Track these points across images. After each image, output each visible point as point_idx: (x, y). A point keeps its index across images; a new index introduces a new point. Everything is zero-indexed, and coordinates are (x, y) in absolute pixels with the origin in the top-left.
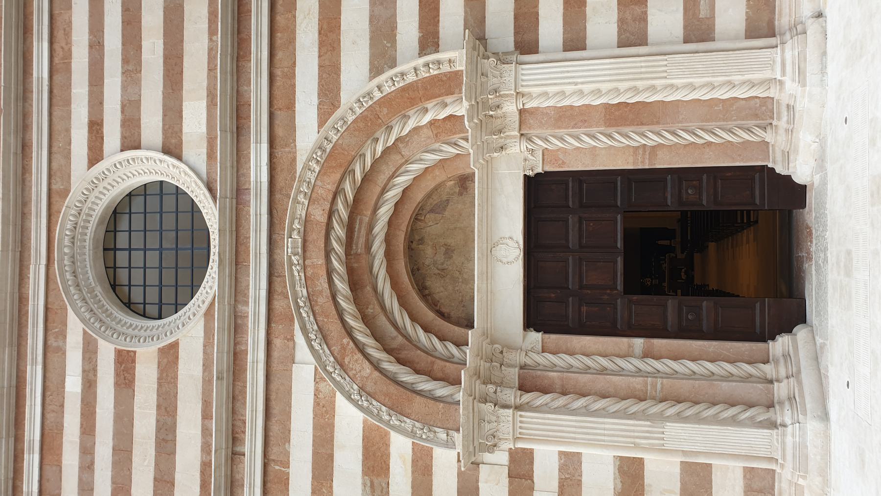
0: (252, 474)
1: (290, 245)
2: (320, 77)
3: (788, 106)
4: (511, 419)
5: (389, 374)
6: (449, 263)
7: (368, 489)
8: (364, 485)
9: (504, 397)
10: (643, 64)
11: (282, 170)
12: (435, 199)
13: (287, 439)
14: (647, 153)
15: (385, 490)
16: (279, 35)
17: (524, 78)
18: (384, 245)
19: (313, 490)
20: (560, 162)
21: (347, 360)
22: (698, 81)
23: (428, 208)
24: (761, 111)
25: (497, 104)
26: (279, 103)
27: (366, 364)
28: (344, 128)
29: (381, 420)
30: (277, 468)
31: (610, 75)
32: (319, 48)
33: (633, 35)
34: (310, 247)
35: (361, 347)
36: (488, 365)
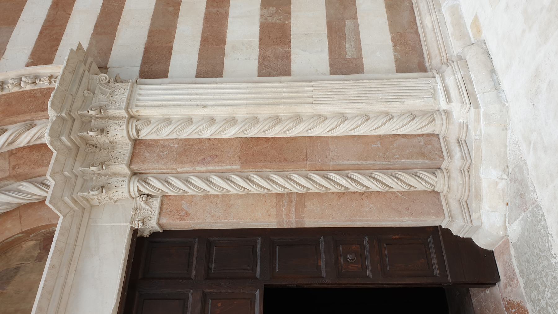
3: (458, 141)
10: (285, 90)
14: (293, 204)
17: (141, 92)
20: (183, 213)
22: (348, 109)
24: (426, 151)
31: (247, 99)
33: (275, 57)
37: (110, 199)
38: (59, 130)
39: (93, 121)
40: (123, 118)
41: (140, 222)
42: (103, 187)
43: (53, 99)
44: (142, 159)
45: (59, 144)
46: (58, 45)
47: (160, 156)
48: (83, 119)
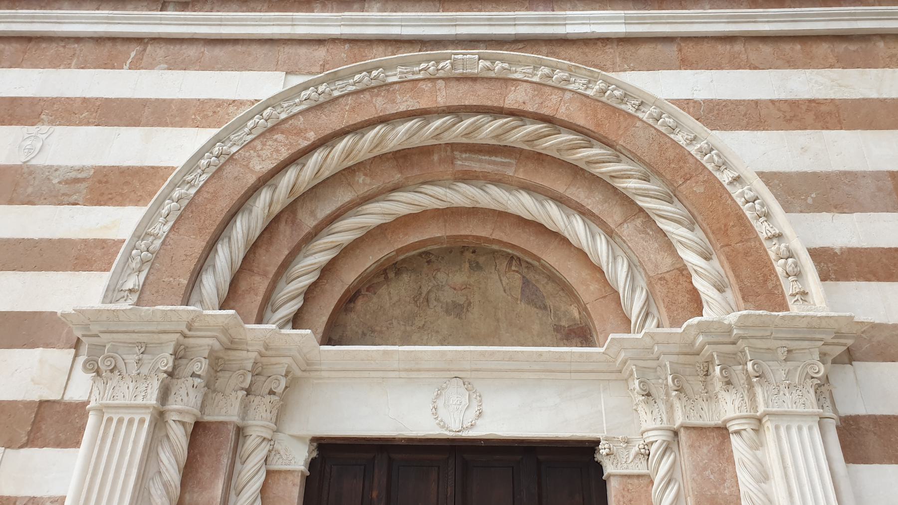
0: (129, 21)
1: (472, 61)
2: (738, 103)
4: (139, 401)
5: (250, 202)
6: (438, 309)
7: (73, 175)
8: (81, 170)
9: (183, 392)
11: (584, 53)
12: (546, 288)
13: (172, 66)
15: (66, 199)
16: (798, 47)
17: (805, 431)
18: (468, 204)
19: (89, 99)
21: (279, 137)
23: (531, 276)
25: (735, 380)
26: (690, 50)
27: (269, 165)
28: (663, 129)
29: (174, 186)
30: (133, 54)
32: (786, 101)
34: (464, 87)
35: (300, 161)
36: (249, 366)
37: (637, 404)
38: (712, 330)
39: (741, 367)
40: (756, 409)
41: (607, 450)
42: (649, 395)
43: (755, 315)
44: (697, 444)
45: (693, 333)
46: (879, 280)
47: (705, 469)
48: (740, 354)
